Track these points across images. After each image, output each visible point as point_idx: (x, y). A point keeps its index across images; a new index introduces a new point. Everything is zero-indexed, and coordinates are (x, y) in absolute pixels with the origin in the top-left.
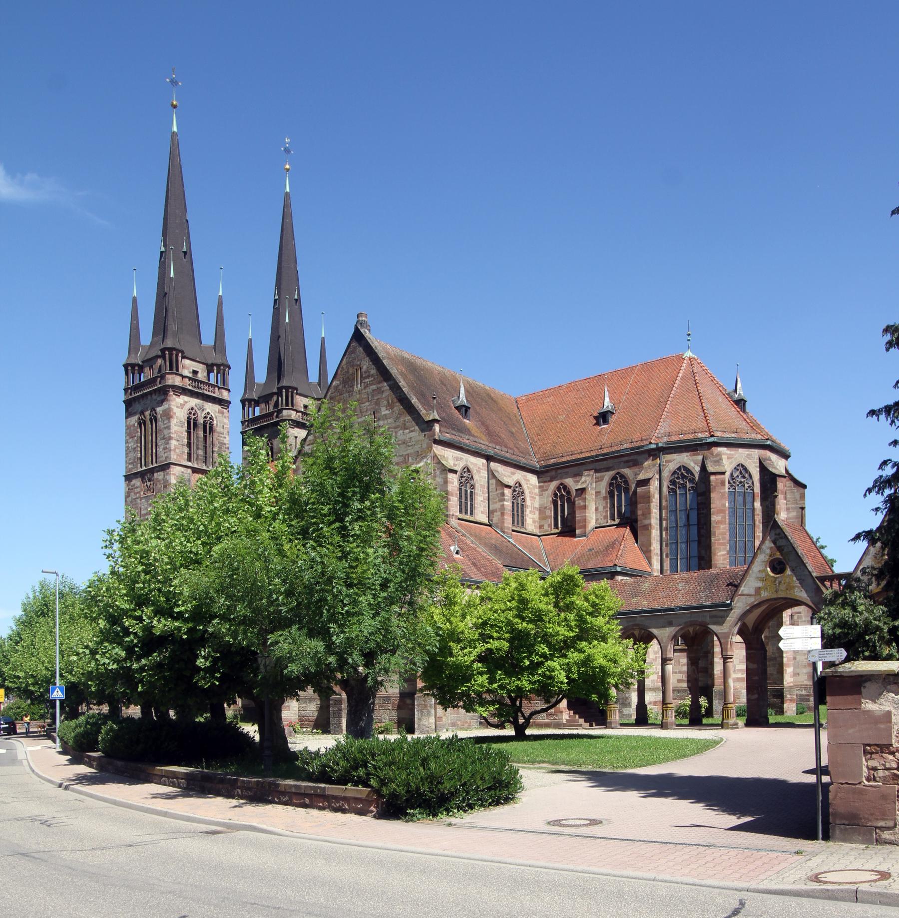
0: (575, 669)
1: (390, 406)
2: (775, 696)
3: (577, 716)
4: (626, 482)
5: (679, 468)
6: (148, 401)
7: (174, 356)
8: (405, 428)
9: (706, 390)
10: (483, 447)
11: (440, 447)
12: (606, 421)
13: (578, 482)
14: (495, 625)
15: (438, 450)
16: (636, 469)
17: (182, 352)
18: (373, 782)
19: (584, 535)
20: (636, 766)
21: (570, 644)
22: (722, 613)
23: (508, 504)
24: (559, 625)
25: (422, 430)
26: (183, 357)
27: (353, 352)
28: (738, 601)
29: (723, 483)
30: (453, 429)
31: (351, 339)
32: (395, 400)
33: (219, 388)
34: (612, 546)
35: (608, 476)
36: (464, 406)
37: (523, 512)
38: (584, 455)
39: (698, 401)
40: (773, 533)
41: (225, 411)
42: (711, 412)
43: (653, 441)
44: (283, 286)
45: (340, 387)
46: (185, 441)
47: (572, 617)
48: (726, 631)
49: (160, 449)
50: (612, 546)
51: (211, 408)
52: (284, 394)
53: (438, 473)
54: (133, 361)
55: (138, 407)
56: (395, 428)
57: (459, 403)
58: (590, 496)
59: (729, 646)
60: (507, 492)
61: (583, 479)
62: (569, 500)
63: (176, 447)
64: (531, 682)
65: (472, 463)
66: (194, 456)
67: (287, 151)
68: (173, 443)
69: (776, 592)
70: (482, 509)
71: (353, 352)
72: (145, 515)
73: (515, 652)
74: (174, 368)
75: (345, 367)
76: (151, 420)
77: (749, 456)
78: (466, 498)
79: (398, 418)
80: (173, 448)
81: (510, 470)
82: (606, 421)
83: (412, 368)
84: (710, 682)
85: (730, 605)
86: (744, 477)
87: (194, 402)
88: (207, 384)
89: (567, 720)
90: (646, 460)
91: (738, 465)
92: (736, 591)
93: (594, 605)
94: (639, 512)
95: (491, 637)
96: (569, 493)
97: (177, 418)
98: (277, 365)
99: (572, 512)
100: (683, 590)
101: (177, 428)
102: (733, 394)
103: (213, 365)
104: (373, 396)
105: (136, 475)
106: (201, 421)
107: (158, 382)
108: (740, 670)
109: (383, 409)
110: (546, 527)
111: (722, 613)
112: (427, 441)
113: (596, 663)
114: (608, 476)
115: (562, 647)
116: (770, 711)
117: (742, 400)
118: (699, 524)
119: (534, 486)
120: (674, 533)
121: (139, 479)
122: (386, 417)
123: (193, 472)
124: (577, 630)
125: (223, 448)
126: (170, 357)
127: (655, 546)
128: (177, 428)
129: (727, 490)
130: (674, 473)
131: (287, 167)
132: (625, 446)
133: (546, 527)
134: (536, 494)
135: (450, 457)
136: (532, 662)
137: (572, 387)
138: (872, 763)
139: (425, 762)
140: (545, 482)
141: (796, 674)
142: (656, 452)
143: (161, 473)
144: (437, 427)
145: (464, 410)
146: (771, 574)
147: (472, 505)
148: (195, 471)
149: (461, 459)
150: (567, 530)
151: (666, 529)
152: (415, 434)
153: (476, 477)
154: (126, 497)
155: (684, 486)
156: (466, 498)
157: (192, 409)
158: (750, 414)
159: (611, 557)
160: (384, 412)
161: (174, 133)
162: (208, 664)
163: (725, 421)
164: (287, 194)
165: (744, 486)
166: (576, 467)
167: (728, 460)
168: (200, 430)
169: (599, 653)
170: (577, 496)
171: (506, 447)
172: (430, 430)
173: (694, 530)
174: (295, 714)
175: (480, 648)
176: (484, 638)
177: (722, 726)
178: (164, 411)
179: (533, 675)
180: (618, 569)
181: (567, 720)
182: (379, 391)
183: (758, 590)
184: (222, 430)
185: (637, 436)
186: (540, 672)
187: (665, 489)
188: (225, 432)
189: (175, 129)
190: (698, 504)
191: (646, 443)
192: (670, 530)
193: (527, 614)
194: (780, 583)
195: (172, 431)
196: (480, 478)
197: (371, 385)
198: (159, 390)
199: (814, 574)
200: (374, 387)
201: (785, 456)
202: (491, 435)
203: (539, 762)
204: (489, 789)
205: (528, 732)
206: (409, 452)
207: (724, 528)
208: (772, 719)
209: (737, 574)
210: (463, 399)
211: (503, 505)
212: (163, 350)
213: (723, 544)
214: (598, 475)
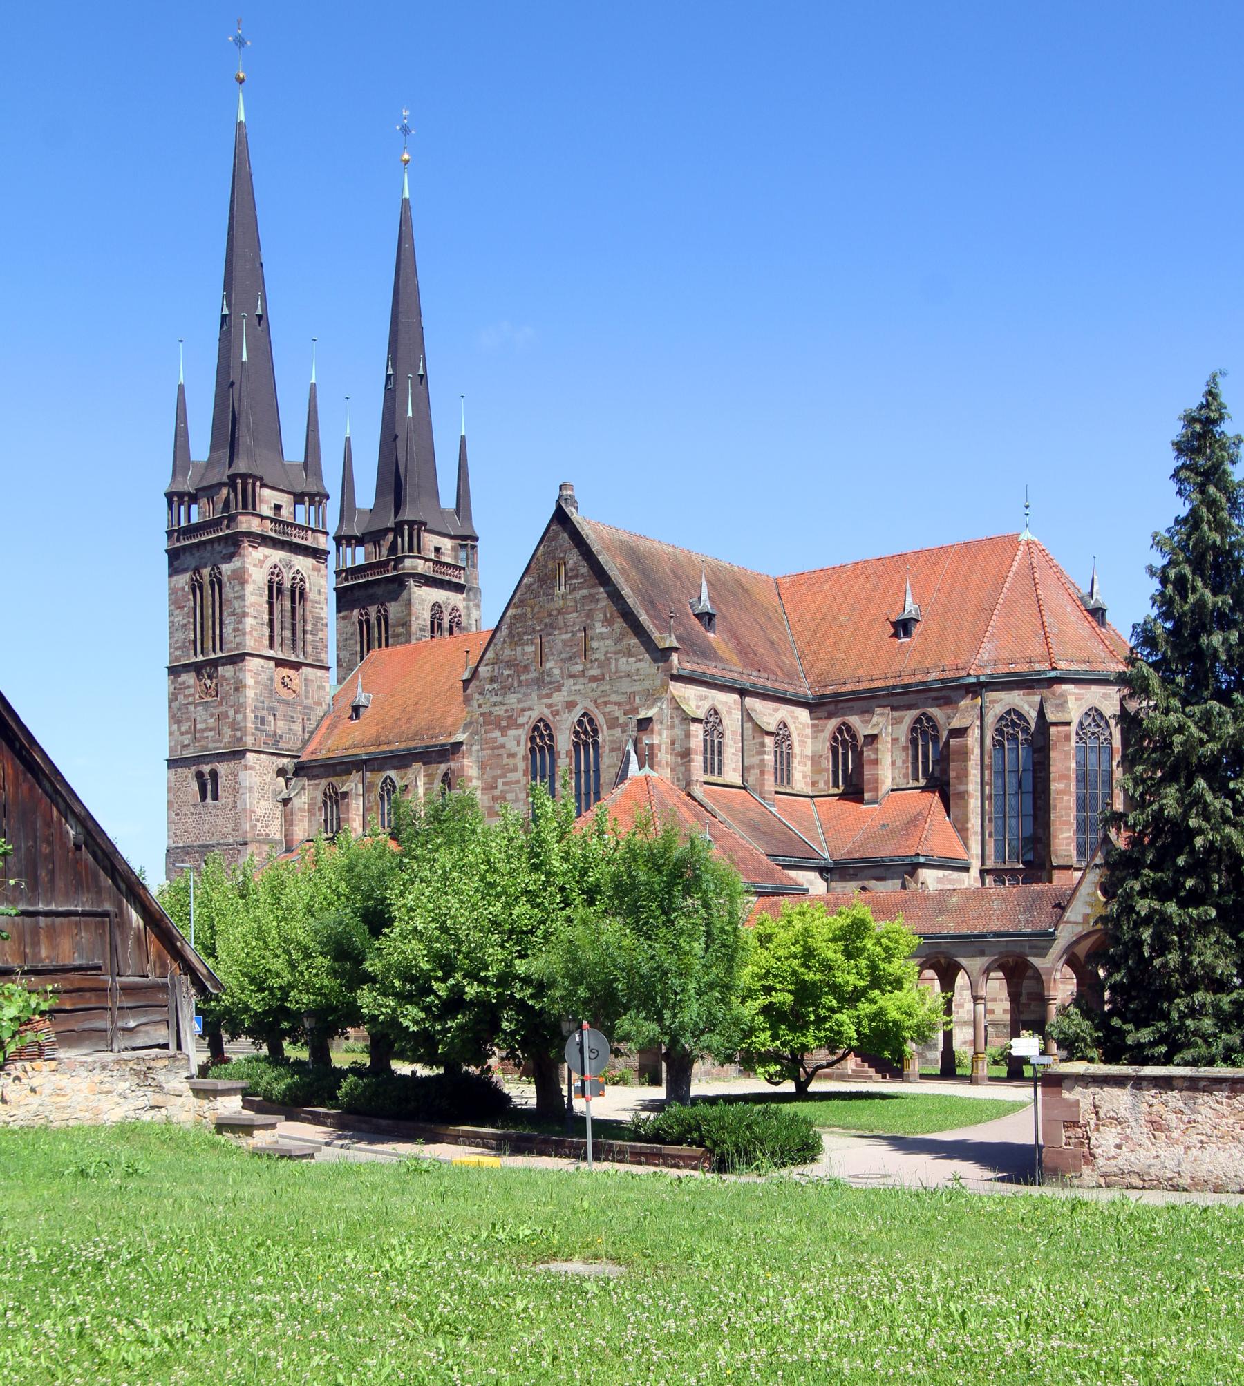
0: (865, 1022)
1: (608, 622)
3: (866, 1065)
4: (935, 727)
7: (250, 487)
9: (1051, 595)
10: (735, 676)
11: (678, 685)
12: (907, 633)
13: (868, 722)
15: (677, 689)
16: (949, 711)
17: (261, 479)
18: (707, 1143)
20: (928, 1132)
21: (858, 995)
22: (1044, 944)
23: (769, 758)
24: (848, 973)
26: (262, 486)
27: (554, 538)
29: (1067, 738)
30: (694, 652)
31: (551, 521)
32: (616, 614)
34: (914, 822)
35: (910, 716)
36: (707, 613)
39: (1036, 612)
41: (322, 566)
42: (1055, 630)
43: (972, 672)
44: (401, 353)
45: (535, 586)
46: (266, 617)
47: (863, 963)
49: (228, 630)
50: (914, 822)
52: (406, 532)
55: (189, 560)
56: (616, 653)
57: (700, 609)
58: (884, 745)
60: (769, 741)
61: (875, 720)
62: (854, 747)
63: (253, 629)
64: (817, 1038)
65: (721, 702)
66: (277, 640)
67: (405, 130)
68: (249, 621)
70: (734, 766)
71: (554, 538)
72: (203, 730)
73: (801, 1006)
74: (249, 503)
75: (542, 559)
77: (1105, 696)
78: (713, 751)
81: (772, 705)
82: (907, 633)
83: (636, 557)
85: (1053, 934)
86: (1098, 726)
87: (277, 556)
89: (853, 1071)
90: (963, 698)
91: (1091, 709)
92: (1061, 916)
93: (887, 949)
94: (952, 774)
95: (776, 990)
96: (854, 737)
97: (255, 582)
98: (394, 484)
99: (859, 765)
100: (1003, 910)
101: (254, 598)
102: (1086, 599)
103: (303, 495)
104: (583, 605)
105: (187, 667)
106: (287, 584)
107: (224, 526)
110: (821, 784)
111: (1044, 944)
112: (661, 675)
113: (889, 1017)
114: (910, 716)
115: (852, 998)
118: (1034, 791)
120: (1000, 803)
121: (192, 674)
122: (601, 637)
123: (277, 666)
126: (243, 488)
127: (974, 822)
128: (254, 598)
130: (1002, 718)
131: (406, 157)
132: (934, 676)
133: (821, 784)
134: (807, 736)
135: (692, 697)
136: (817, 1016)
137: (859, 569)
138: (1069, 1134)
139: (749, 1127)
142: (976, 689)
143: (230, 667)
144: (675, 657)
145: (707, 619)
147: (720, 760)
148: (280, 663)
149: (706, 697)
150: (851, 790)
151: (990, 798)
152: (645, 664)
154: (171, 701)
155: (1014, 738)
157: (275, 567)
158: (1113, 626)
160: (599, 628)
161: (240, 123)
162: (513, 1027)
164: (405, 203)
165: (1098, 738)
166: (866, 700)
168: (287, 596)
169: (891, 1004)
170: (864, 744)
172: (666, 661)
173: (1028, 800)
175: (762, 1001)
176: (768, 990)
178: (234, 571)
180: (922, 860)
181: (853, 1071)
184: (317, 597)
185: (950, 662)
187: (988, 741)
188: (322, 600)
189: (242, 117)
190: (1034, 764)
192: (994, 798)
193: (812, 962)
195: (248, 603)
196: (732, 722)
197: (580, 588)
198: (225, 538)
200: (585, 592)
202: (744, 651)
203: (830, 1126)
204: (799, 1150)
205: (814, 1087)
206: (635, 689)
209: (1064, 893)
210: (705, 604)
211: (763, 760)
212: (233, 478)
213: (1068, 823)
214: (896, 714)
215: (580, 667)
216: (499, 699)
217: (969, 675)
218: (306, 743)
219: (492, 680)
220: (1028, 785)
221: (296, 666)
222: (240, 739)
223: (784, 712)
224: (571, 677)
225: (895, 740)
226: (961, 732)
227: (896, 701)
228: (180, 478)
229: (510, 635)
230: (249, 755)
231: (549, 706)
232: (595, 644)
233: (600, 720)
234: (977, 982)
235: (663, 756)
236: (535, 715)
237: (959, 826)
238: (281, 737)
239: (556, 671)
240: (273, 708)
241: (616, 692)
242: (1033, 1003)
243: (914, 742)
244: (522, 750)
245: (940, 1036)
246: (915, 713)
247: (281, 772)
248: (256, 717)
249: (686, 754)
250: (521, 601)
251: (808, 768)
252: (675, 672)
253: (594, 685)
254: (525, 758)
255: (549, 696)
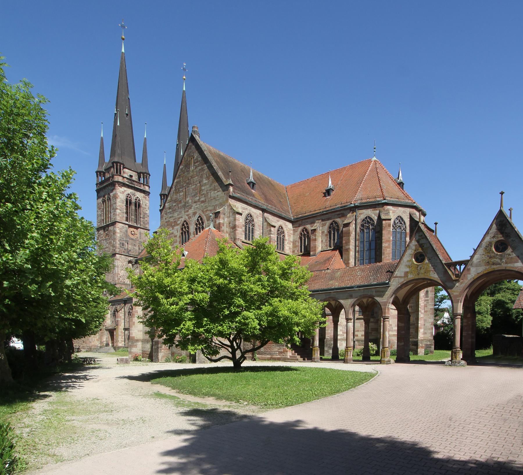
1: (208, 178)
2: (413, 345)
3: (296, 354)
4: (338, 226)
5: (366, 218)
6: (106, 190)
8: (215, 190)
9: (382, 176)
11: (233, 201)
14: (201, 281)
15: (232, 202)
16: (343, 219)
19: (314, 255)
21: (263, 300)
24: (254, 284)
25: (223, 191)
26: (124, 168)
27: (190, 149)
28: (393, 281)
29: (389, 225)
30: (243, 192)
33: (144, 185)
35: (328, 223)
36: (252, 182)
37: (283, 243)
38: (316, 212)
40: (417, 235)
46: (125, 211)
48: (385, 301)
49: (112, 214)
51: (139, 195)
53: (231, 214)
54: (100, 170)
55: (102, 193)
56: (210, 190)
57: (249, 181)
58: (319, 233)
59: (387, 311)
61: (315, 224)
65: (253, 212)
67: (184, 69)
68: (118, 211)
69: (418, 274)
74: (119, 173)
76: (108, 200)
77: (404, 212)
78: (249, 232)
79: (211, 184)
80: (118, 214)
81: (276, 219)
84: (378, 336)
85: (388, 283)
86: (401, 223)
87: (129, 191)
88: (138, 183)
89: (290, 357)
90: (349, 213)
94: (344, 242)
97: (120, 198)
101: (120, 203)
103: (141, 173)
106: (133, 201)
108: (395, 330)
109: (204, 180)
110: (296, 252)
113: (280, 314)
114: (328, 223)
116: (411, 353)
117: (402, 183)
119: (290, 230)
122: (205, 184)
124: (269, 289)
125: (146, 216)
126: (117, 166)
128: (120, 203)
129: (391, 230)
130: (364, 220)
131: (184, 77)
132: (338, 206)
133: (296, 252)
137: (314, 179)
140: (296, 227)
141: (425, 333)
144: (231, 189)
145: (252, 185)
146: (416, 263)
148: (130, 226)
149: (246, 209)
152: (220, 193)
153: (255, 220)
155: (368, 228)
156: (249, 232)
159: (326, 265)
160: (205, 181)
163: (392, 192)
165: (401, 228)
167: (393, 213)
168: (133, 206)
171: (275, 206)
174: (140, 350)
177: (380, 362)
178: (114, 195)
179: (232, 322)
182: (202, 170)
183: (406, 274)
185: (344, 201)
186: (237, 320)
187: (358, 229)
188: (147, 208)
191: (348, 204)
194: (421, 268)
195: (117, 205)
197: (198, 166)
199: (444, 262)
200: (200, 168)
201: (424, 215)
202: (267, 199)
206: (217, 203)
207: (390, 251)
208: (412, 358)
209: (393, 265)
210: (252, 179)
211: (270, 237)
215: (198, 198)
216: (172, 215)
217: (351, 203)
218: (140, 253)
219: (170, 208)
220: (373, 246)
221: (137, 228)
222: (115, 250)
223: (281, 222)
224: (195, 202)
225: (323, 232)
226: (347, 225)
227: (323, 217)
228: (100, 167)
229: (176, 190)
230: (117, 255)
231: (188, 215)
232: (203, 188)
233: (205, 218)
234: (349, 311)
235: (225, 228)
236: (183, 219)
237: (346, 262)
238: (130, 250)
239: (190, 201)
240: (127, 241)
241: (210, 206)
242: (373, 332)
243: (330, 232)
244: (179, 234)
245: (317, 330)
246: (331, 221)
247: (130, 262)
248: (120, 243)
249: (234, 228)
250: (179, 176)
251: (291, 245)
252: (231, 195)
253: (203, 204)
254: (180, 236)
255: (188, 211)
